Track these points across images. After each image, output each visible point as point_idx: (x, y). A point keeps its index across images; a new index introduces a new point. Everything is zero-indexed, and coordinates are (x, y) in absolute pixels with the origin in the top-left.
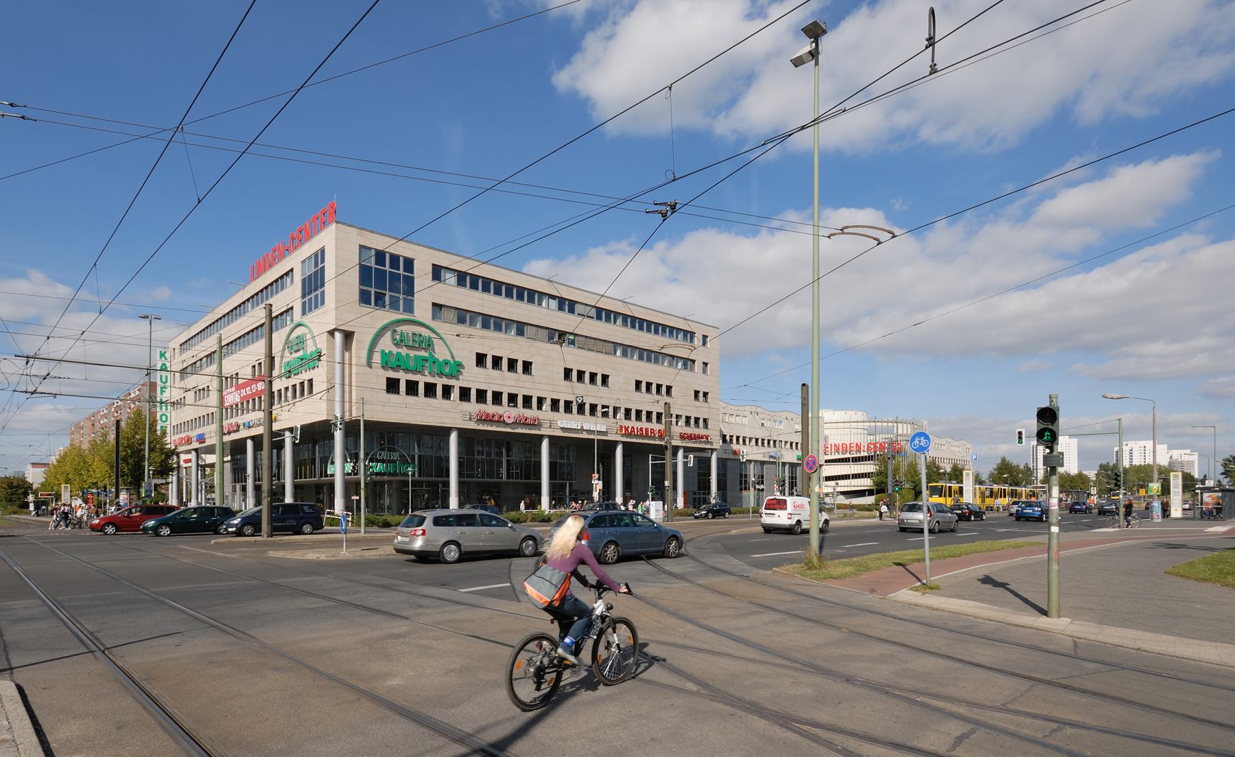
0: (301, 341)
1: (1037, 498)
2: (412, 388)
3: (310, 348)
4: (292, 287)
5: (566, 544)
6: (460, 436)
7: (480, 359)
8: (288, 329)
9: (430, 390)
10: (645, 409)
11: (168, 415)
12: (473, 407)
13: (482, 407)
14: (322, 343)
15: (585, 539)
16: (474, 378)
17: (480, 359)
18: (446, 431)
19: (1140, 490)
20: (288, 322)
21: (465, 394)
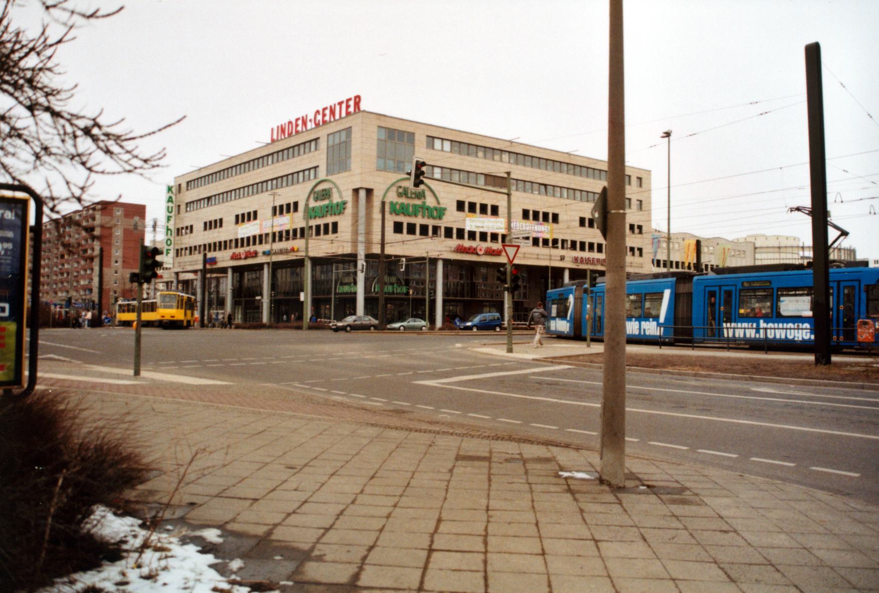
0: (326, 194)
1: (340, 208)
2: (411, 229)
3: (336, 199)
4: (317, 152)
5: (117, 533)
6: (444, 265)
7: (460, 206)
8: (313, 183)
9: (424, 230)
10: (587, 240)
11: (172, 240)
12: (454, 242)
13: (460, 242)
14: (348, 197)
15: (120, 546)
16: (453, 218)
17: (460, 206)
18: (434, 261)
19: (629, 269)
20: (312, 176)
21: (448, 233)
